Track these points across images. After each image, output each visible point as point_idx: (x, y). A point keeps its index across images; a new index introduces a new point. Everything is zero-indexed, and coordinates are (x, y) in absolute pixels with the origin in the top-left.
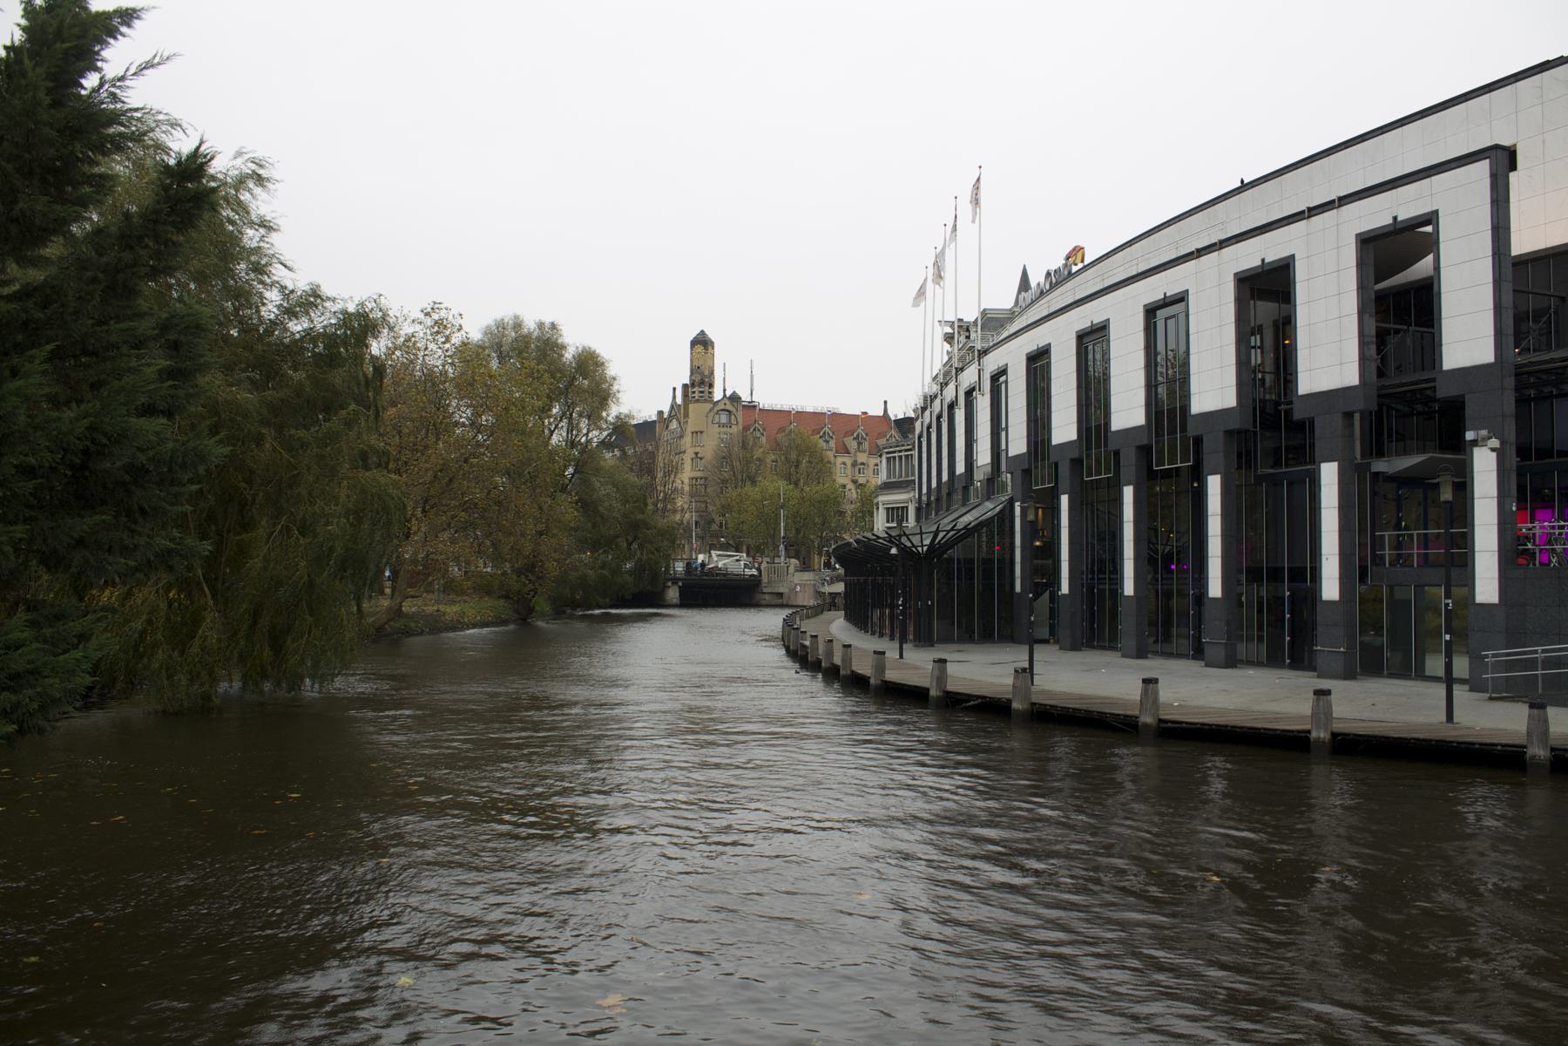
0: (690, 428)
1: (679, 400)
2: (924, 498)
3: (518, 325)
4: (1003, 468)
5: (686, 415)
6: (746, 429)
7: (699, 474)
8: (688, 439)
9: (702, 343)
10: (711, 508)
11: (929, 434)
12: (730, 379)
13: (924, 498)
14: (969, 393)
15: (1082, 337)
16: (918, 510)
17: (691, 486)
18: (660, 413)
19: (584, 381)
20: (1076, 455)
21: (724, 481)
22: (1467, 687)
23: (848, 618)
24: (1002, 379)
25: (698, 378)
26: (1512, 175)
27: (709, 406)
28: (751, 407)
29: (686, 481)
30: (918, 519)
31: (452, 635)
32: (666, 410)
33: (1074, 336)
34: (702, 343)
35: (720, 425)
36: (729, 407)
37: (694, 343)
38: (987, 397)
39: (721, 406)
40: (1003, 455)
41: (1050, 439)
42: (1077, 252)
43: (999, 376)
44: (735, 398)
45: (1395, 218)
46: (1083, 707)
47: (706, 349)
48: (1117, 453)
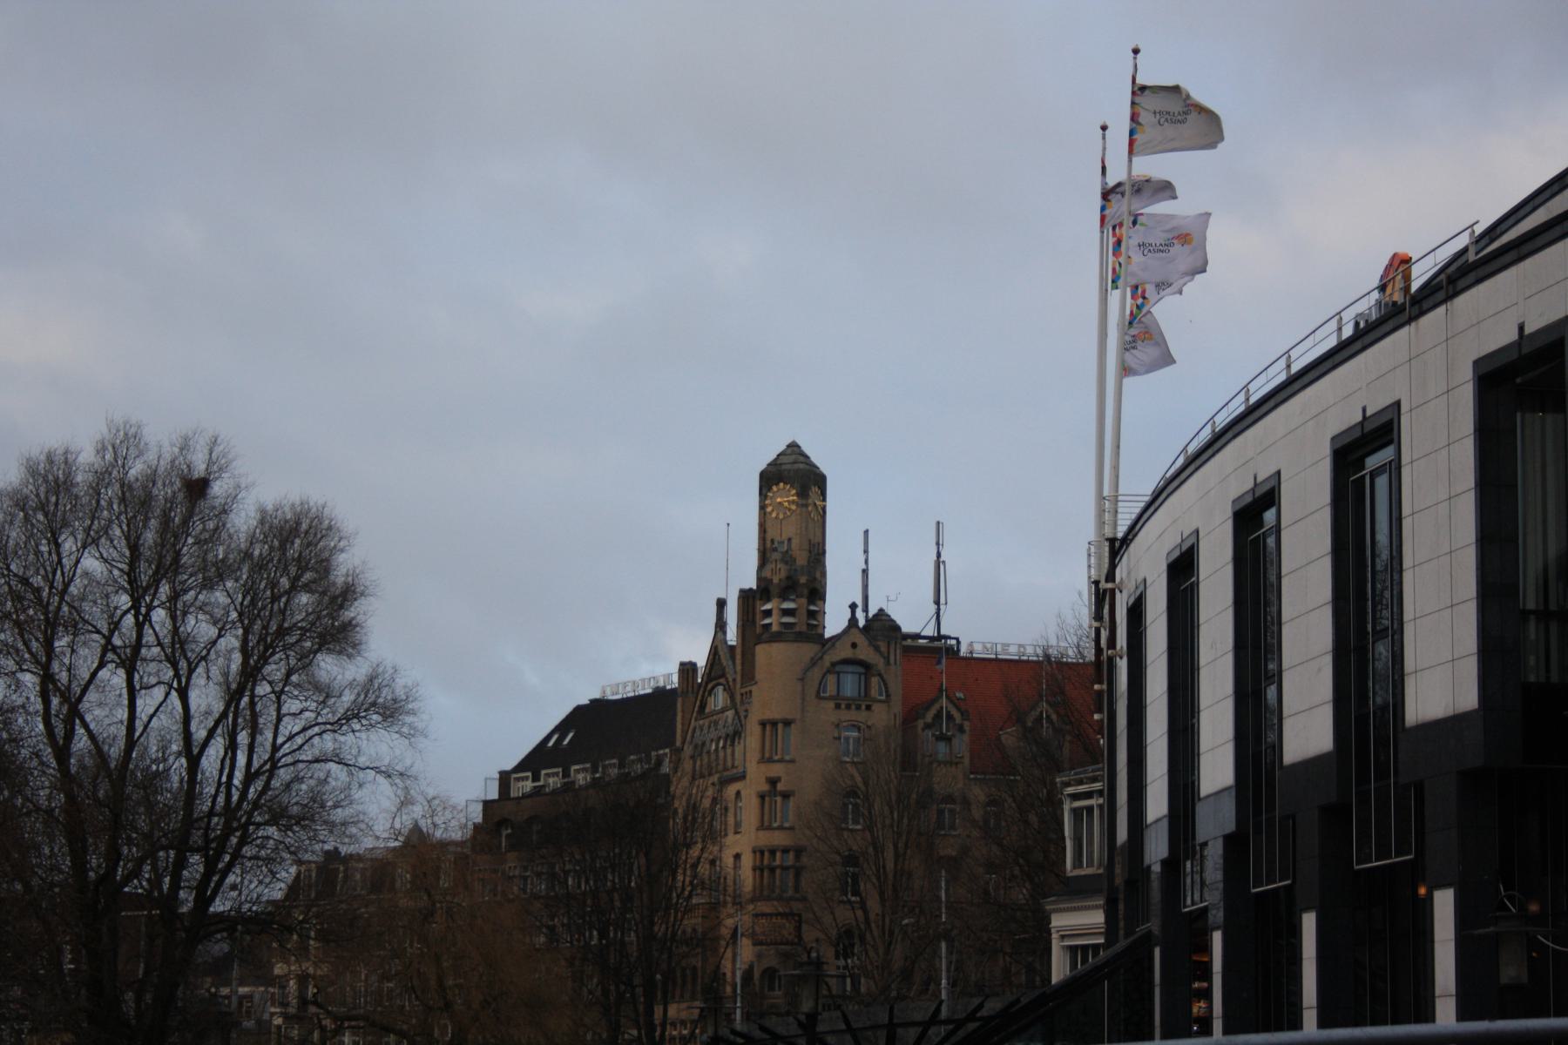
0: (757, 713)
1: (732, 636)
5: (749, 676)
6: (910, 717)
7: (779, 839)
8: (752, 738)
9: (794, 480)
10: (809, 934)
12: (876, 569)
17: (758, 869)
18: (687, 669)
21: (851, 860)
22: (494, 794)
25: (778, 576)
26: (751, 583)
27: (808, 650)
28: (939, 650)
29: (747, 861)
32: (701, 660)
34: (794, 480)
35: (839, 702)
36: (865, 653)
37: (770, 478)
39: (844, 652)
41: (1278, 747)
42: (1401, 263)
44: (881, 628)
45: (1521, 328)
47: (803, 493)
48: (1420, 788)
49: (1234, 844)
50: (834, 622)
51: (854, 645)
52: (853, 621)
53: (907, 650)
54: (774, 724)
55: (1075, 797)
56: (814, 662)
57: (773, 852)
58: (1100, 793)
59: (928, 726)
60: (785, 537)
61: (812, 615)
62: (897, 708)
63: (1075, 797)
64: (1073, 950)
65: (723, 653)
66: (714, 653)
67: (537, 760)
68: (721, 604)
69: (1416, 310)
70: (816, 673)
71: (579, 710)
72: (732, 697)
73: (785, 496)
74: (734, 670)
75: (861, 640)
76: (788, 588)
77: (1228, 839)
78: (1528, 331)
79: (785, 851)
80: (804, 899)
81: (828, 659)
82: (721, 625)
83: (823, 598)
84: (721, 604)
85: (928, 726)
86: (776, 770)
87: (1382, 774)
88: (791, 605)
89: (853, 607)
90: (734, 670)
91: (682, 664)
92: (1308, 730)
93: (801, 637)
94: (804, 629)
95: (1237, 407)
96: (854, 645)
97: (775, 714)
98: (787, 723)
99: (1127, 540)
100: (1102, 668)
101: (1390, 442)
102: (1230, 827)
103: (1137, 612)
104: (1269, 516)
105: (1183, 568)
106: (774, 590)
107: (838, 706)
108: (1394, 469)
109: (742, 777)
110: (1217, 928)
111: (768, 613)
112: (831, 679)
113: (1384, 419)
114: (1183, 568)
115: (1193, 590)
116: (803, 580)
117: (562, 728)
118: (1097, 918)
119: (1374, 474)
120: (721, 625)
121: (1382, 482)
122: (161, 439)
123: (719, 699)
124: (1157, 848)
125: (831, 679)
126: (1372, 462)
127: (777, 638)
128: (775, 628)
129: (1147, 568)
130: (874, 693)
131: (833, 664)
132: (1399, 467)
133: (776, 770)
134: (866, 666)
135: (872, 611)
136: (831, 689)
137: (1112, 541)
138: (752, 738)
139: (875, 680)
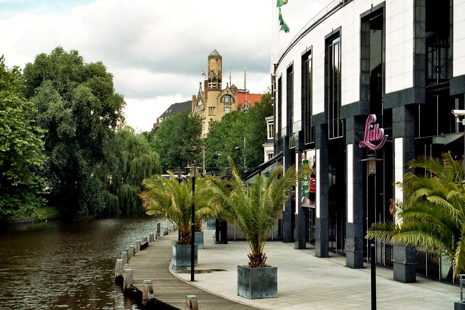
1: (203, 90)
5: (206, 98)
8: (207, 110)
27: (218, 92)
36: (230, 93)
47: (217, 60)
49: (301, 133)
50: (224, 86)
51: (228, 92)
52: (227, 86)
53: (238, 92)
54: (211, 108)
55: (270, 122)
56: (219, 95)
58: (272, 122)
61: (219, 85)
62: (236, 104)
63: (270, 122)
64: (269, 155)
65: (201, 93)
66: (199, 93)
67: (164, 115)
69: (346, 3)
70: (220, 97)
71: (176, 104)
73: (213, 61)
74: (203, 97)
75: (229, 90)
76: (214, 80)
77: (299, 132)
78: (373, 6)
81: (222, 95)
83: (221, 82)
86: (211, 117)
87: (336, 117)
88: (215, 83)
89: (227, 84)
90: (203, 97)
92: (318, 107)
93: (216, 90)
95: (303, 31)
96: (228, 92)
97: (212, 106)
98: (214, 108)
99: (278, 65)
100: (274, 94)
101: (339, 36)
102: (301, 130)
103: (280, 80)
104: (310, 57)
105: (290, 70)
106: (211, 80)
107: (224, 104)
108: (340, 43)
109: (205, 119)
111: (210, 85)
112: (223, 98)
113: (337, 31)
114: (290, 70)
115: (292, 75)
117: (169, 109)
118: (272, 148)
121: (336, 47)
123: (200, 103)
124: (284, 133)
126: (334, 42)
127: (212, 90)
128: (211, 88)
129: (282, 71)
130: (232, 101)
133: (211, 117)
134: (230, 96)
135: (232, 84)
136: (223, 101)
137: (275, 65)
138: (207, 110)
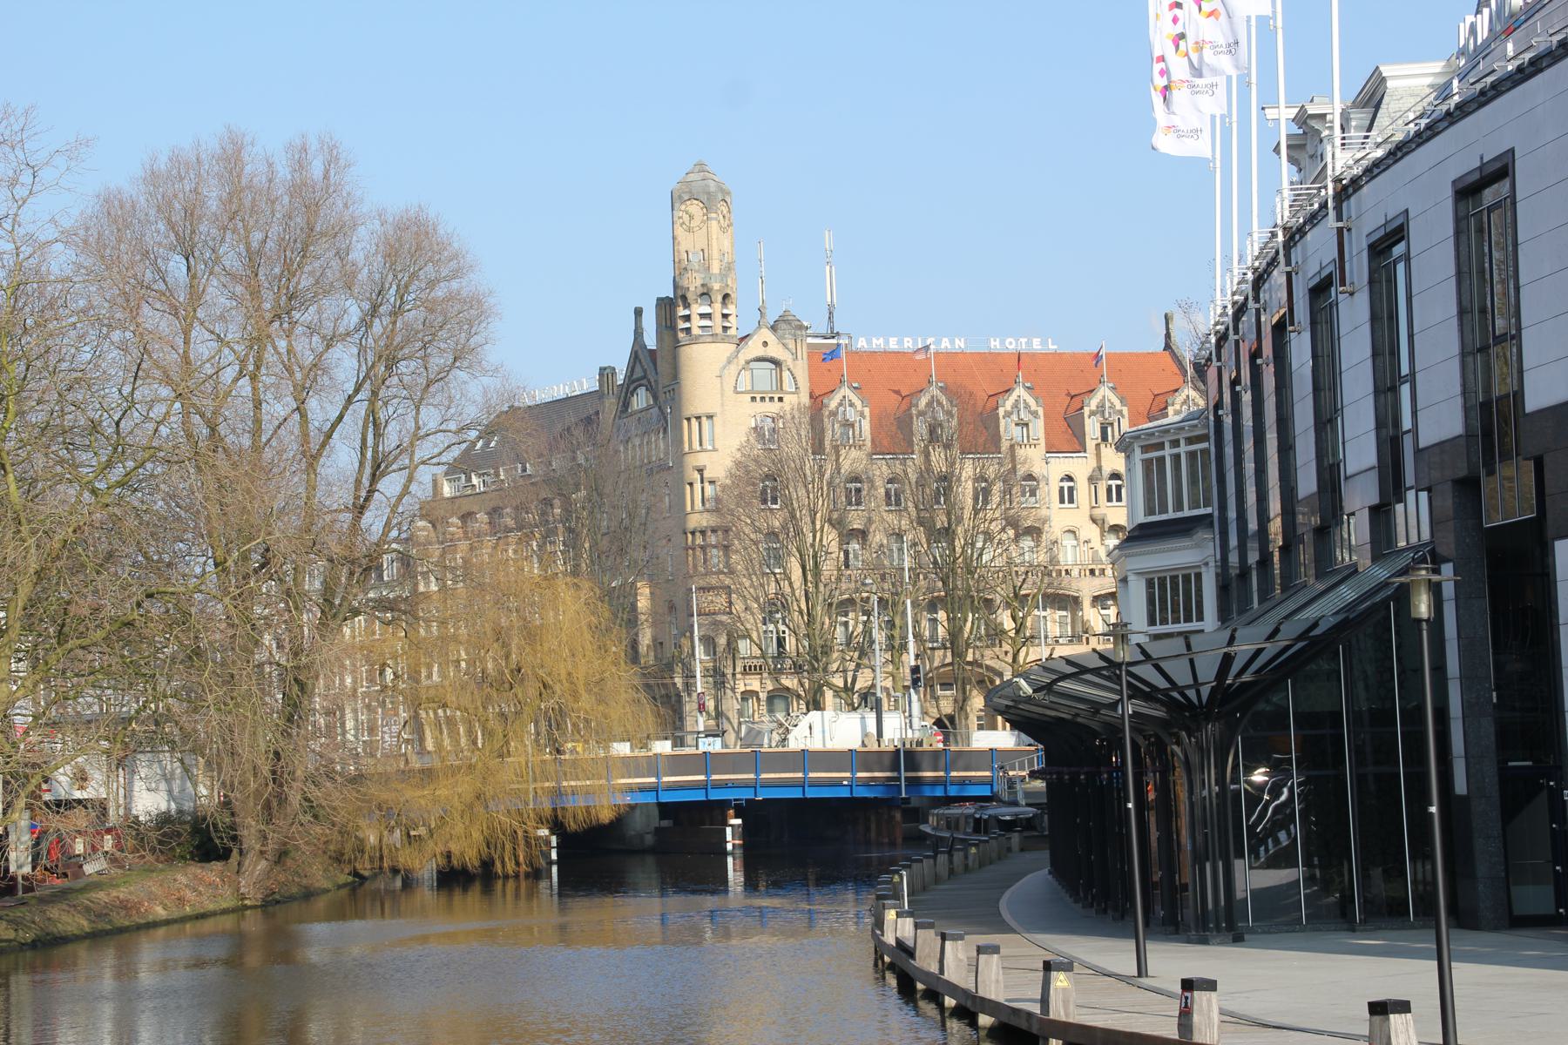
1: (651, 341)
2: (1234, 559)
3: (232, 158)
4: (1410, 479)
11: (1236, 398)
13: (1234, 559)
14: (1320, 290)
15: (1467, 191)
16: (1223, 589)
18: (606, 373)
19: (416, 308)
20: (1462, 472)
23: (1060, 870)
24: (1398, 250)
30: (1224, 614)
31: (107, 1026)
33: (1448, 192)
38: (1362, 301)
40: (1408, 442)
43: (1388, 243)
46: (597, 900)
57: (703, 532)
59: (1092, 413)
60: (698, 248)
66: (635, 357)
68: (638, 312)
70: (733, 369)
72: (655, 398)
79: (714, 531)
80: (732, 572)
82: (638, 333)
84: (638, 312)
85: (1092, 413)
91: (602, 370)
94: (720, 330)
110: (1447, 561)
111: (687, 318)
116: (716, 286)
119: (1490, 210)
120: (638, 333)
122: (270, 148)
125: (746, 375)
130: (786, 387)
131: (748, 362)
132: (1514, 203)
134: (776, 363)
139: (786, 374)
